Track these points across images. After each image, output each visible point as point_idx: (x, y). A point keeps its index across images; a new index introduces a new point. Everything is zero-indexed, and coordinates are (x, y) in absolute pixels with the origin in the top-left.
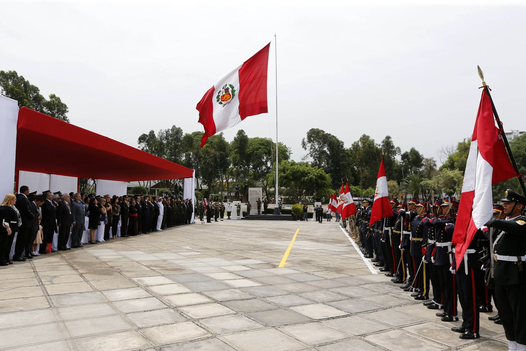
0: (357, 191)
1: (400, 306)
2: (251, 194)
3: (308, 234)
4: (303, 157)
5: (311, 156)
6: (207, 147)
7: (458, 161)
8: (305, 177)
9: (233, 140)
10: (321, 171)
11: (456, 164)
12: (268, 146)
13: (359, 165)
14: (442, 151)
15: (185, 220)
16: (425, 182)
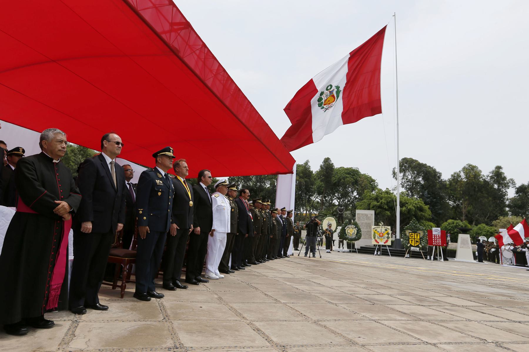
12: (353, 175)
15: (276, 250)
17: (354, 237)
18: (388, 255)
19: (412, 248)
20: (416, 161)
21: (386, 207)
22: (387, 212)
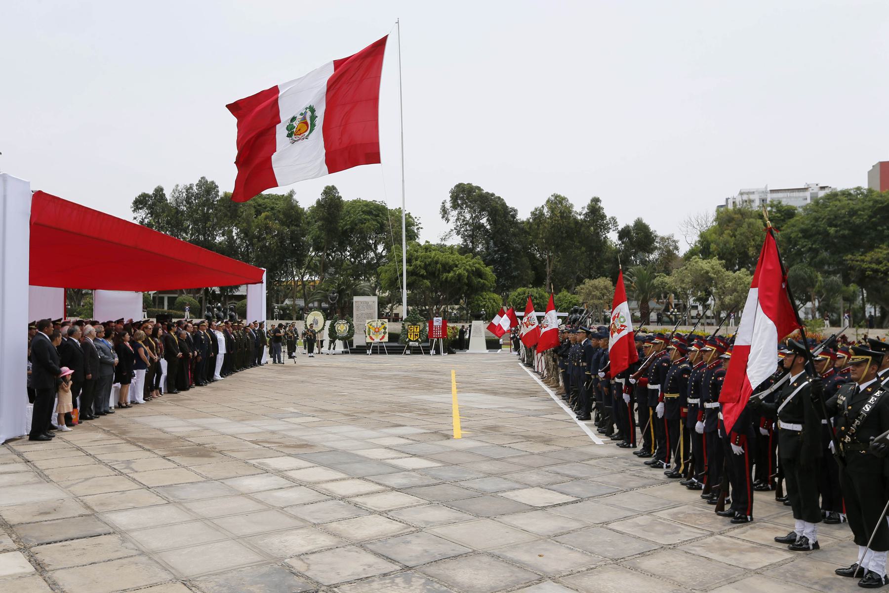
0: (541, 297)
1: (644, 486)
2: (358, 307)
3: (473, 379)
4: (442, 235)
5: (458, 233)
6: (267, 218)
7: (715, 242)
8: (449, 272)
9: (314, 203)
10: (477, 263)
11: (713, 247)
12: (378, 215)
13: (542, 250)
14: (689, 223)
16: (661, 279)
17: (345, 334)
18: (385, 353)
19: (411, 343)
20: (478, 188)
21: (423, 272)
22: (425, 281)
